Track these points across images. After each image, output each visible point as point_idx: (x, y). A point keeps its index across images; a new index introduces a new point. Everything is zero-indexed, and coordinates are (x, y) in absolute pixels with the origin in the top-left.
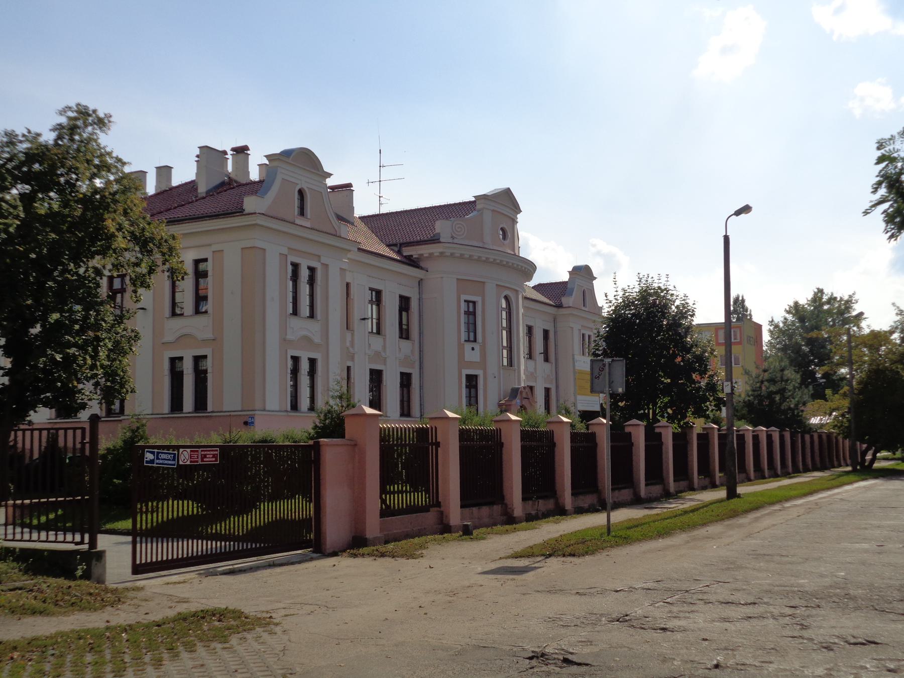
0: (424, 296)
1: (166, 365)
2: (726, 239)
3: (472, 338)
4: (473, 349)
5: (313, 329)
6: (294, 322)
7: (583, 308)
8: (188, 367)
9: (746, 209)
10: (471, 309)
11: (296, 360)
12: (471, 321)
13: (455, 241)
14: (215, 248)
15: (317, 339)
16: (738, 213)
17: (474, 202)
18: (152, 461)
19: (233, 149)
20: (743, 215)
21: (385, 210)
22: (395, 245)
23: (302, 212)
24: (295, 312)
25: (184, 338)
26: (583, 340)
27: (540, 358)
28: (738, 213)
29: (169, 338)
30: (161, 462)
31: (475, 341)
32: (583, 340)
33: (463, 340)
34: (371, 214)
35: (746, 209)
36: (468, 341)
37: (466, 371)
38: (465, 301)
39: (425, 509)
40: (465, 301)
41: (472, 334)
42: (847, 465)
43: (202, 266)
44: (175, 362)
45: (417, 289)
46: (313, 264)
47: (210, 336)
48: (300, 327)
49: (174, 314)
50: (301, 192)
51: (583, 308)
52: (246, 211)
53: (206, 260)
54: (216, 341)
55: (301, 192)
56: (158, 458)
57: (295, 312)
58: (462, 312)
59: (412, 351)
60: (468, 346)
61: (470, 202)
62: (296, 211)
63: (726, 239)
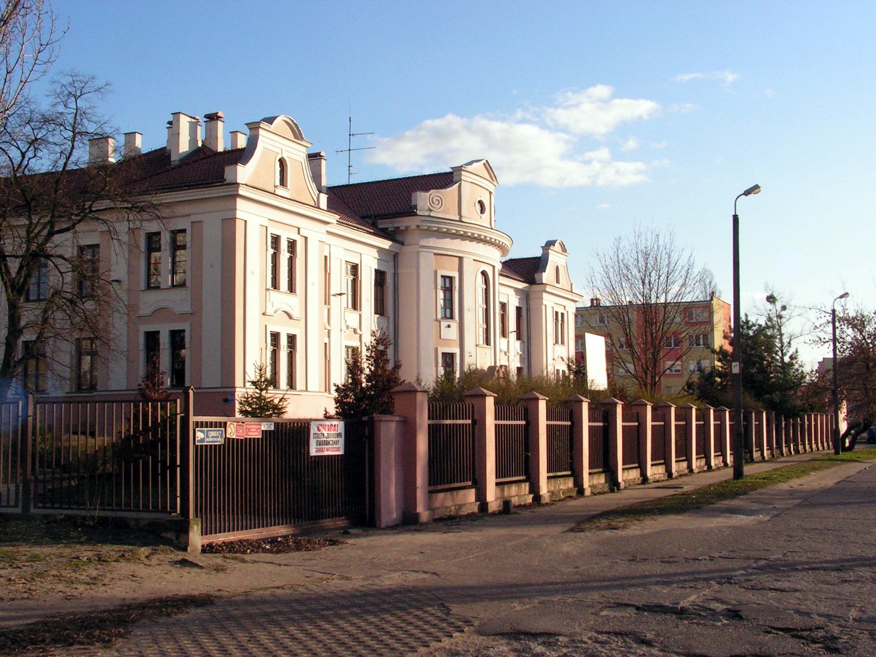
0: (400, 271)
1: (142, 340)
2: (736, 219)
3: (448, 315)
4: (449, 326)
5: (293, 303)
6: (273, 294)
7: (557, 285)
8: (165, 340)
9: (754, 189)
10: (448, 285)
11: (275, 337)
12: (448, 297)
13: (432, 214)
14: (194, 218)
15: (295, 314)
16: (747, 193)
17: (451, 173)
18: (202, 440)
19: (207, 116)
20: (751, 196)
21: (353, 181)
22: (370, 217)
23: (283, 182)
24: (275, 285)
25: (160, 312)
26: (557, 319)
27: (513, 336)
28: (747, 193)
29: (145, 310)
30: (211, 439)
31: (452, 317)
32: (557, 319)
33: (439, 317)
34: (341, 184)
35: (754, 189)
36: (445, 317)
37: (442, 350)
38: (442, 276)
39: (8, 503)
40: (442, 276)
41: (448, 311)
42: (318, 450)
43: (180, 237)
44: (152, 339)
45: (392, 264)
46: (294, 236)
47: (188, 309)
48: (281, 299)
49: (149, 287)
50: (282, 162)
51: (557, 285)
52: (228, 181)
53: (184, 231)
54: (195, 314)
55: (282, 162)
56: (208, 437)
57: (275, 285)
58: (439, 287)
59: (388, 328)
60: (444, 324)
61: (446, 174)
62: (278, 183)
63: (736, 219)
